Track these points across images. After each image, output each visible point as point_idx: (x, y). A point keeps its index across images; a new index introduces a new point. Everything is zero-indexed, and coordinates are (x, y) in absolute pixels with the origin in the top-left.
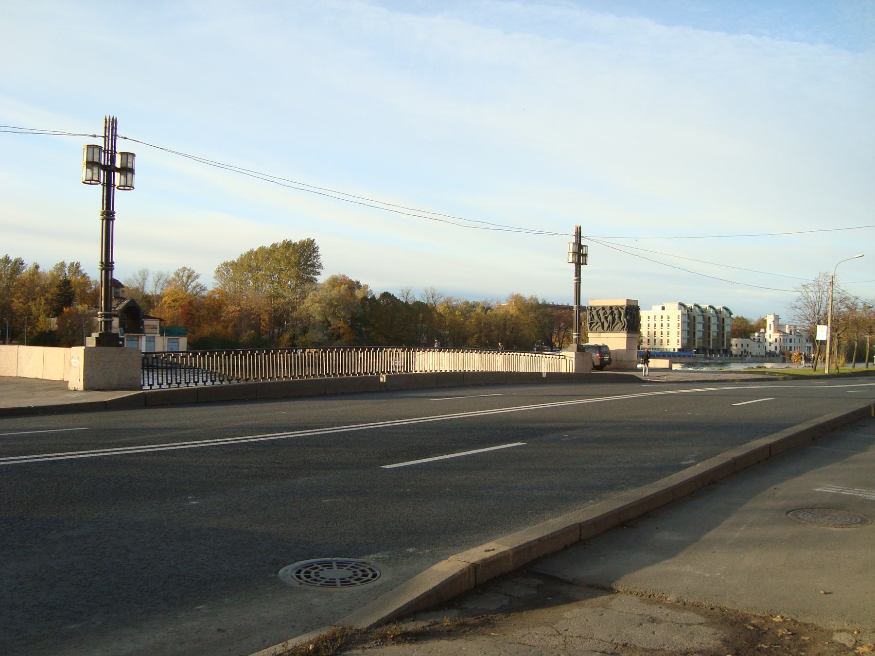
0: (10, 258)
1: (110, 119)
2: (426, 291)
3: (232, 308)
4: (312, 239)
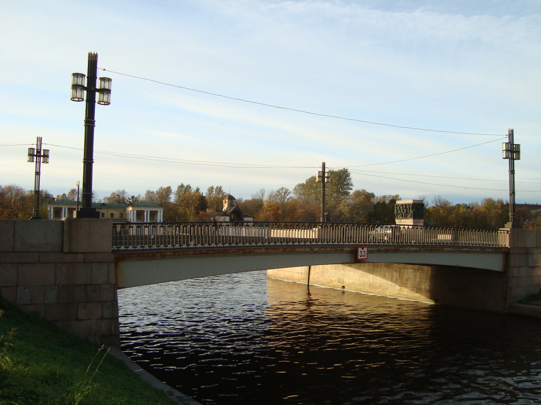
0: (184, 185)
2: (435, 198)
3: (300, 211)
4: (346, 169)
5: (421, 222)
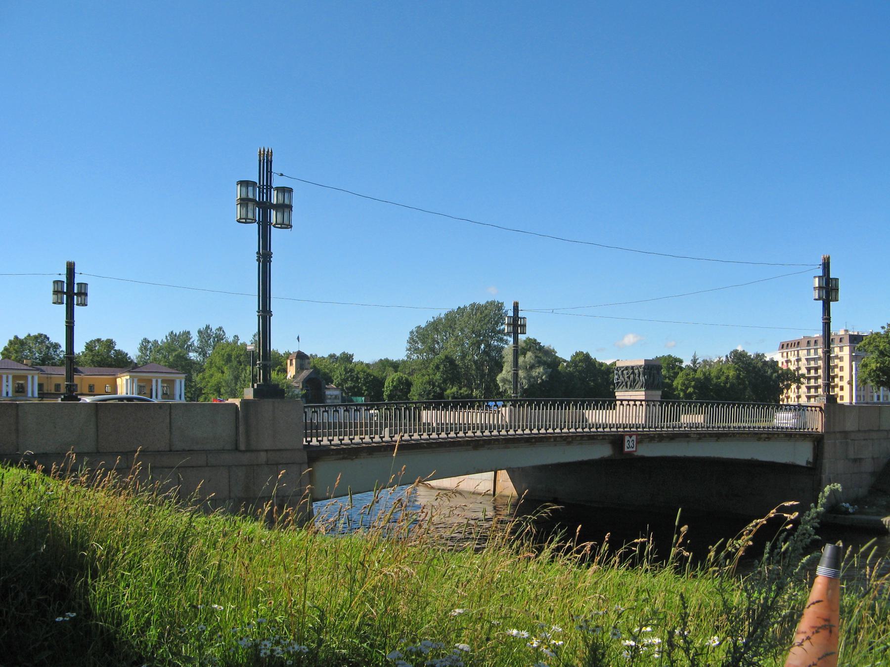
1: (264, 151)
5: (657, 394)
